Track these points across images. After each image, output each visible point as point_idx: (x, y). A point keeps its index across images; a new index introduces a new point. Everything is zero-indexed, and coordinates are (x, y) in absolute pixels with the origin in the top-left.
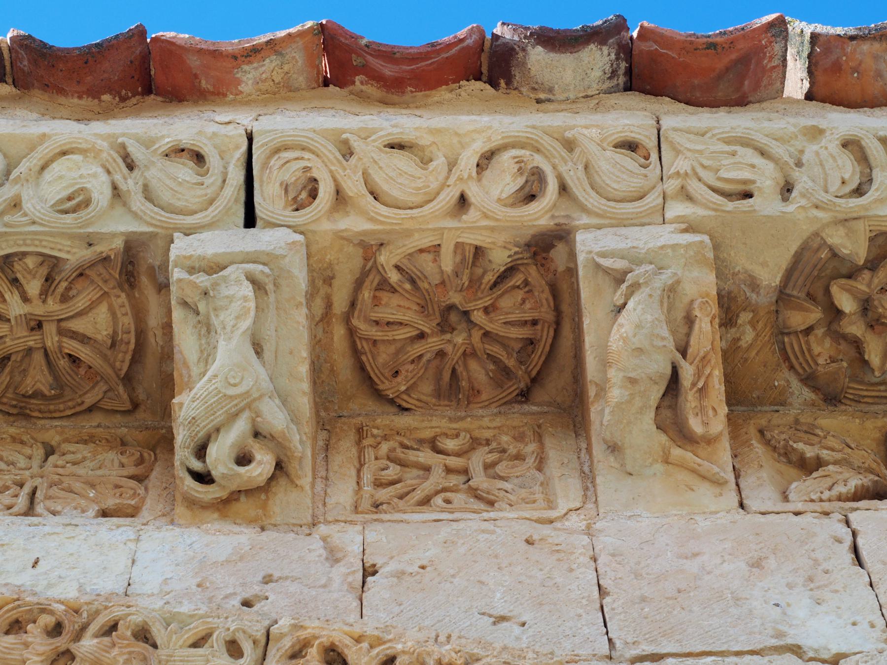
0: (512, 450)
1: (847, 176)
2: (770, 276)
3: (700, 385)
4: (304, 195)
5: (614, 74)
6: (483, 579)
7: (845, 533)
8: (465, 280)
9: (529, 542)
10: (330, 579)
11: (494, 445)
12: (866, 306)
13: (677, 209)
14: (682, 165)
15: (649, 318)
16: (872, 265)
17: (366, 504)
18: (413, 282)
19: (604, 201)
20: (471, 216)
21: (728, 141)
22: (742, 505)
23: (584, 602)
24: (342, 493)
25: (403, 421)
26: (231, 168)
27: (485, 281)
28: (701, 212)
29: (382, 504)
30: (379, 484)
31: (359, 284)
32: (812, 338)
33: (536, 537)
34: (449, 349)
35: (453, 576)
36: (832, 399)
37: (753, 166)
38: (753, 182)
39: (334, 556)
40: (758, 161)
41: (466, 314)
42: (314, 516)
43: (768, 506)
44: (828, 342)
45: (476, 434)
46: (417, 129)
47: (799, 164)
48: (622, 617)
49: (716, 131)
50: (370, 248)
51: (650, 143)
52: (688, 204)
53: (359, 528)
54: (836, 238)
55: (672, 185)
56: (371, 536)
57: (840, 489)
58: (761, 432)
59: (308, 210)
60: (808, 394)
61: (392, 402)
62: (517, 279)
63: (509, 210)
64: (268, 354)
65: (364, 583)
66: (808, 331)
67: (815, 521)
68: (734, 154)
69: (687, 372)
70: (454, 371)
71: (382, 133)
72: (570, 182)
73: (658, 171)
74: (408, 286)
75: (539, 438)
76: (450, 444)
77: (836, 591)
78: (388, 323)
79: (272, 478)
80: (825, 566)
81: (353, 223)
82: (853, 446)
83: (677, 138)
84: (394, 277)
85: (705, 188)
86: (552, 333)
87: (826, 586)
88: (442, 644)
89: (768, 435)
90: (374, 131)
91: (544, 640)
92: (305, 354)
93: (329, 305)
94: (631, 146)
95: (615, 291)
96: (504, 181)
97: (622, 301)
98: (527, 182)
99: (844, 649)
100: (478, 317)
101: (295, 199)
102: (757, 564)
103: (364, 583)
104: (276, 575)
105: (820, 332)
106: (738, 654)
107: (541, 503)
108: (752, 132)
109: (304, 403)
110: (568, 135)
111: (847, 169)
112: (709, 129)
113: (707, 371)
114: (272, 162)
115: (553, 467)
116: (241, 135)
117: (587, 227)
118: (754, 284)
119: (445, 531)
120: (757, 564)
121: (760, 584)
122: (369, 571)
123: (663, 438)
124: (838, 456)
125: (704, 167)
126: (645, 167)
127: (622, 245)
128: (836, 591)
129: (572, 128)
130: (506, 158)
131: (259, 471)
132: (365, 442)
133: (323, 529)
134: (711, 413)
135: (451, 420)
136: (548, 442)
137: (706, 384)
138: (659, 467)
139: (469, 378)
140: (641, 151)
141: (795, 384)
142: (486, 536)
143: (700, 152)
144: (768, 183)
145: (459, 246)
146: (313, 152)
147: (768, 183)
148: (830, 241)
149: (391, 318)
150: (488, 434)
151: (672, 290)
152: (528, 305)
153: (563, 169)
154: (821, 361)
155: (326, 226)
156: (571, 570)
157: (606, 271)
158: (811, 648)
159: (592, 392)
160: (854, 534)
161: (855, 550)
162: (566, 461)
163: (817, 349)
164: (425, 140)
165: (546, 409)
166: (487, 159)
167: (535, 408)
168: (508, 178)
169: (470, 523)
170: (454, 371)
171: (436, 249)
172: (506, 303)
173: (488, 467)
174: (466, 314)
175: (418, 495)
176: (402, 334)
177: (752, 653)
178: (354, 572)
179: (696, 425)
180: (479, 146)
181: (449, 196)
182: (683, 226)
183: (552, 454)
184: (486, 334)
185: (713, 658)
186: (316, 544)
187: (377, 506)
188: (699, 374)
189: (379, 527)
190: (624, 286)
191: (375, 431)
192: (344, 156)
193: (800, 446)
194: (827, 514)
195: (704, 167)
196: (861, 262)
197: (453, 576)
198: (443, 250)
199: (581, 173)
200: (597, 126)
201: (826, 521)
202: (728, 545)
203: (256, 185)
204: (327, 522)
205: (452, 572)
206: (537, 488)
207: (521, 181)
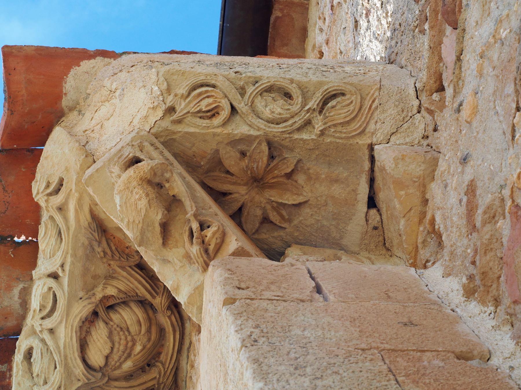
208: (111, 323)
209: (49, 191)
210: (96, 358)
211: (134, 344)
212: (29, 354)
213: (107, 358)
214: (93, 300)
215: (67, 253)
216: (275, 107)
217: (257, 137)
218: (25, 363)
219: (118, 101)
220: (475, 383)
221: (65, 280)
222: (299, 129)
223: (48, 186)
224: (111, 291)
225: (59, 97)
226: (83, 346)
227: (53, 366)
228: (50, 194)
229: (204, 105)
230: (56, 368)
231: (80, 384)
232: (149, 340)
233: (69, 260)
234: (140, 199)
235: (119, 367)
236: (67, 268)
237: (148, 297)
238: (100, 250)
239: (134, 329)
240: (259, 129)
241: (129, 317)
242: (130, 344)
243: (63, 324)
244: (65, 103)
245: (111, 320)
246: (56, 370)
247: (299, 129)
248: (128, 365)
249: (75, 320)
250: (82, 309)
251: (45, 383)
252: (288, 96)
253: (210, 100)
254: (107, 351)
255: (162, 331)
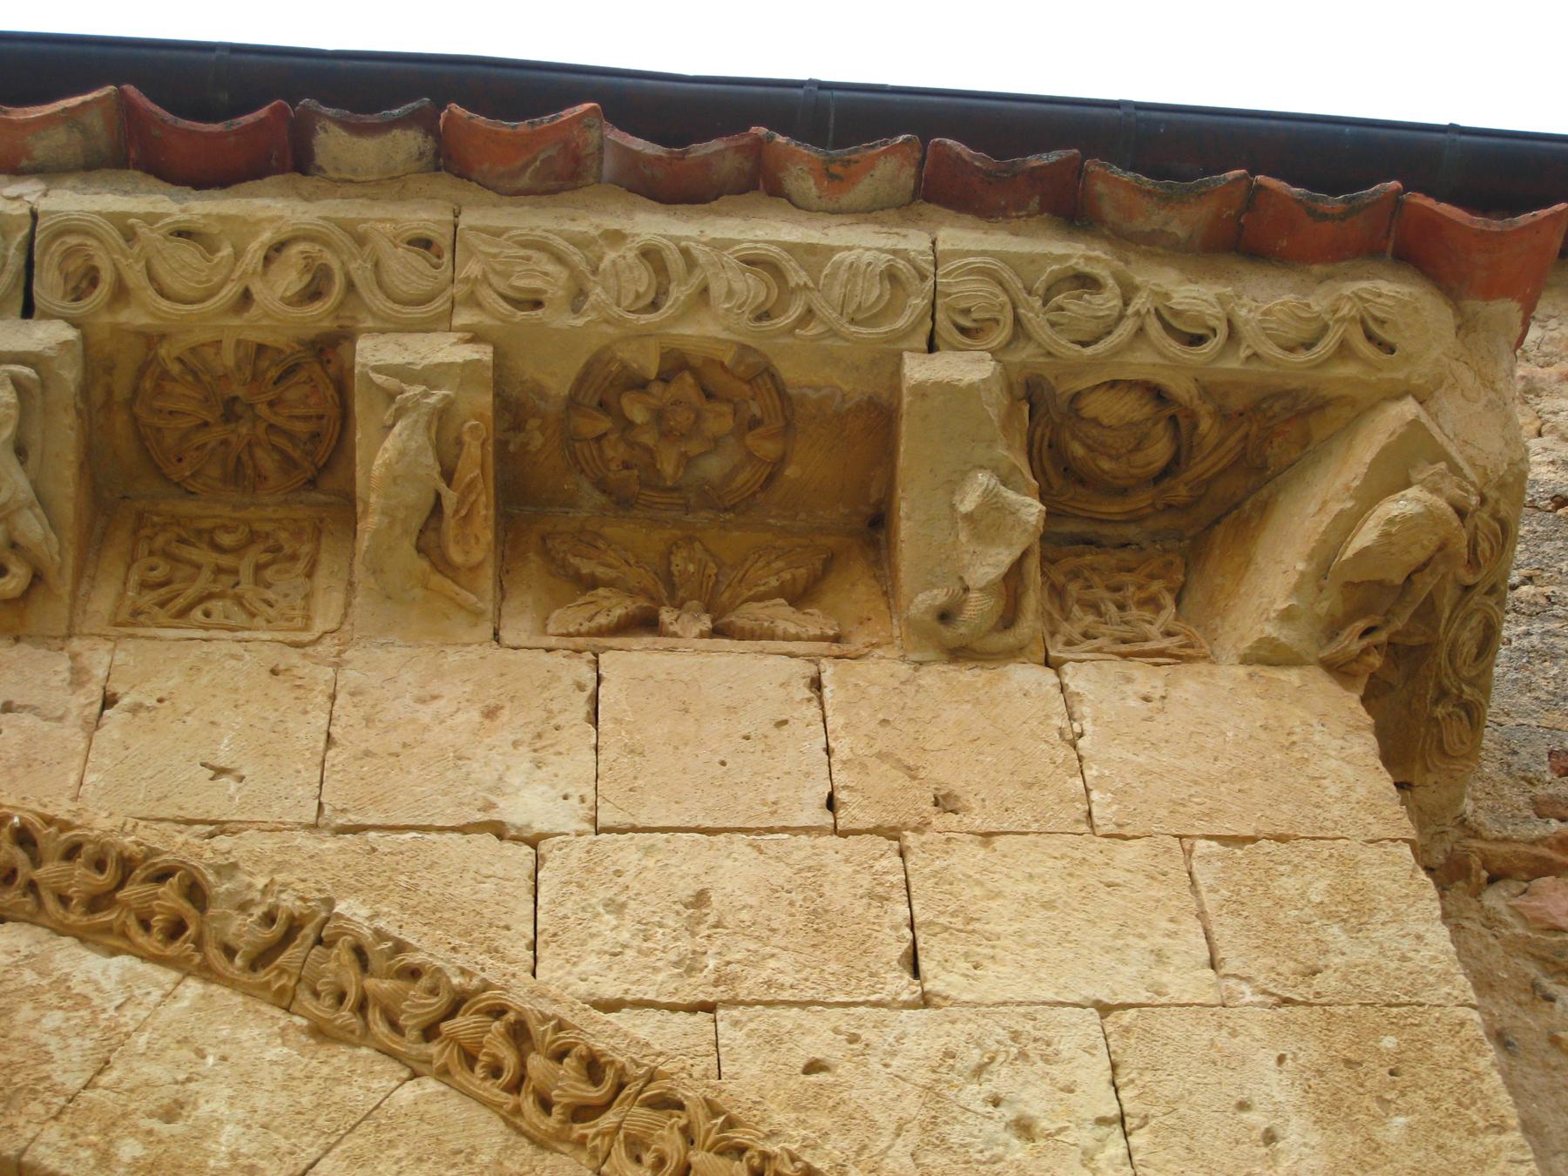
0: (288, 550)
1: (642, 290)
2: (558, 380)
3: (463, 513)
4: (84, 285)
5: (422, 154)
6: (216, 719)
7: (589, 676)
8: (248, 374)
9: (274, 672)
10: (68, 711)
11: (271, 542)
12: (659, 416)
13: (463, 318)
14: (473, 269)
15: (413, 445)
16: (665, 378)
17: (124, 615)
18: (195, 374)
19: (390, 304)
20: (254, 312)
21: (524, 245)
22: (496, 636)
23: (308, 755)
24: (102, 602)
25: (188, 507)
26: (12, 251)
27: (269, 375)
28: (487, 321)
29: (141, 613)
30: (145, 586)
31: (141, 373)
32: (605, 443)
33: (282, 667)
34: (233, 438)
35: (188, 714)
36: (622, 502)
37: (546, 274)
38: (545, 292)
39: (78, 677)
40: (551, 268)
41: (251, 406)
42: (71, 626)
43: (523, 640)
44: (622, 448)
45: (257, 526)
46: (205, 216)
47: (595, 271)
48: (338, 777)
49: (513, 233)
50: (151, 339)
51: (446, 243)
52: (476, 311)
53: (110, 645)
54: (626, 353)
55: (459, 290)
56: (120, 656)
57: (602, 620)
58: (543, 539)
59: (88, 300)
60: (600, 498)
61: (178, 485)
62: (302, 375)
63: (290, 309)
64: (33, 459)
65: (101, 714)
66: (599, 439)
67: (564, 661)
68: (528, 259)
69: (450, 498)
70: (239, 459)
71: (168, 220)
72: (357, 282)
73: (449, 273)
74: (190, 378)
75: (318, 532)
76: (226, 540)
77: (560, 754)
78: (171, 413)
79: (32, 585)
80: (559, 720)
81: (133, 317)
82: (632, 562)
83: (471, 238)
84: (175, 369)
85: (495, 296)
86: (338, 428)
87: (552, 745)
88: (127, 834)
89: (550, 544)
90: (161, 216)
91: (255, 802)
92: (71, 457)
93: (109, 393)
94: (425, 244)
95: (388, 407)
96: (289, 279)
97: (390, 422)
98: (313, 279)
99: (545, 828)
100: (262, 409)
101: (76, 288)
102: (491, 713)
103: (101, 714)
104: (18, 701)
105: (613, 437)
106: (441, 830)
107: (299, 622)
108: (551, 236)
109: (67, 510)
110: (362, 228)
111: (642, 280)
112: (507, 229)
113: (473, 497)
114: (54, 247)
115: (321, 578)
116: (23, 216)
117: (370, 331)
118: (542, 393)
119: (198, 650)
120: (491, 713)
121: (487, 741)
122: (109, 701)
123: (423, 564)
124: (612, 574)
125: (496, 272)
126: (436, 267)
127: (399, 360)
128: (560, 754)
129: (365, 221)
130: (295, 250)
131: (13, 584)
132: (144, 532)
133: (76, 644)
134: (473, 541)
135: (235, 508)
136: (324, 540)
137: (470, 511)
138: (418, 592)
139: (255, 467)
140: (434, 249)
141: (586, 486)
142: (234, 662)
143: (495, 256)
144: (561, 293)
145: (239, 343)
146: (97, 238)
147: (561, 293)
148: (620, 354)
149: (175, 407)
150: (268, 527)
151: (443, 416)
152: (312, 401)
153: (353, 266)
154: (613, 467)
155: (106, 319)
156: (305, 712)
157: (379, 387)
158: (513, 826)
159: (360, 509)
160: (599, 680)
161: (595, 699)
162: (336, 568)
163: (610, 453)
164: (215, 229)
165: (333, 498)
166: (278, 247)
167: (322, 497)
168: (294, 275)
169: (222, 645)
170: (239, 459)
171: (218, 343)
172: (292, 395)
173: (259, 568)
174: (251, 406)
175: (180, 603)
176: (185, 424)
177: (453, 829)
178: (91, 704)
179: (456, 556)
180: (267, 236)
181: (230, 291)
182: (468, 336)
183: (324, 557)
184: (271, 427)
185: (414, 834)
186: (63, 665)
187: (136, 613)
188: (461, 502)
189: (131, 645)
190: (394, 407)
191: (156, 519)
192: (127, 241)
193: (576, 561)
194: (578, 651)
195: (496, 272)
196: (653, 377)
197: (188, 714)
198: (224, 344)
199: (370, 275)
200: (391, 220)
201: (575, 662)
202: (469, 688)
203: (36, 271)
204: (82, 636)
205: (188, 708)
206: (299, 603)
207: (307, 278)
208: (1149, 424)
209: (1371, 323)
210: (1095, 406)
211: (1110, 457)
212: (1086, 282)
213: (1095, 422)
214: (1196, 402)
215: (1277, 366)
216: (1468, 639)
217: (1435, 630)
218: (1071, 273)
219: (1484, 401)
220: (872, 684)
221: (1233, 363)
222: (1439, 685)
223: (1375, 319)
224: (1205, 425)
225: (1489, 293)
226: (1113, 384)
227: (1085, 339)
228: (1363, 322)
229: (1484, 546)
230: (1084, 344)
231: (1053, 382)
232: (1115, 478)
233: (1268, 369)
234: (1423, 547)
235: (1075, 437)
236: (1254, 366)
237: (1189, 475)
238: (1277, 408)
239: (1139, 458)
240: (1446, 632)
241: (1159, 451)
242: (1113, 452)
243: (1158, 360)
244: (1472, 305)
245: (1155, 425)
246: (1078, 347)
247: (1439, 685)
248: (1078, 450)
249: (1162, 378)
250: (1181, 387)
251: (1053, 325)
252: (1479, 655)
253: (1488, 554)
254: (1106, 422)
255: (1124, 492)
